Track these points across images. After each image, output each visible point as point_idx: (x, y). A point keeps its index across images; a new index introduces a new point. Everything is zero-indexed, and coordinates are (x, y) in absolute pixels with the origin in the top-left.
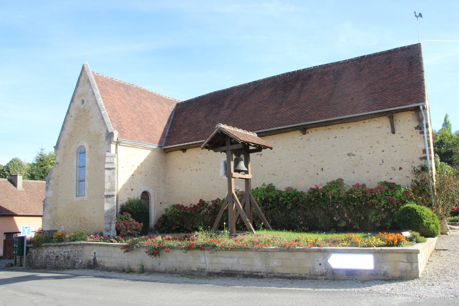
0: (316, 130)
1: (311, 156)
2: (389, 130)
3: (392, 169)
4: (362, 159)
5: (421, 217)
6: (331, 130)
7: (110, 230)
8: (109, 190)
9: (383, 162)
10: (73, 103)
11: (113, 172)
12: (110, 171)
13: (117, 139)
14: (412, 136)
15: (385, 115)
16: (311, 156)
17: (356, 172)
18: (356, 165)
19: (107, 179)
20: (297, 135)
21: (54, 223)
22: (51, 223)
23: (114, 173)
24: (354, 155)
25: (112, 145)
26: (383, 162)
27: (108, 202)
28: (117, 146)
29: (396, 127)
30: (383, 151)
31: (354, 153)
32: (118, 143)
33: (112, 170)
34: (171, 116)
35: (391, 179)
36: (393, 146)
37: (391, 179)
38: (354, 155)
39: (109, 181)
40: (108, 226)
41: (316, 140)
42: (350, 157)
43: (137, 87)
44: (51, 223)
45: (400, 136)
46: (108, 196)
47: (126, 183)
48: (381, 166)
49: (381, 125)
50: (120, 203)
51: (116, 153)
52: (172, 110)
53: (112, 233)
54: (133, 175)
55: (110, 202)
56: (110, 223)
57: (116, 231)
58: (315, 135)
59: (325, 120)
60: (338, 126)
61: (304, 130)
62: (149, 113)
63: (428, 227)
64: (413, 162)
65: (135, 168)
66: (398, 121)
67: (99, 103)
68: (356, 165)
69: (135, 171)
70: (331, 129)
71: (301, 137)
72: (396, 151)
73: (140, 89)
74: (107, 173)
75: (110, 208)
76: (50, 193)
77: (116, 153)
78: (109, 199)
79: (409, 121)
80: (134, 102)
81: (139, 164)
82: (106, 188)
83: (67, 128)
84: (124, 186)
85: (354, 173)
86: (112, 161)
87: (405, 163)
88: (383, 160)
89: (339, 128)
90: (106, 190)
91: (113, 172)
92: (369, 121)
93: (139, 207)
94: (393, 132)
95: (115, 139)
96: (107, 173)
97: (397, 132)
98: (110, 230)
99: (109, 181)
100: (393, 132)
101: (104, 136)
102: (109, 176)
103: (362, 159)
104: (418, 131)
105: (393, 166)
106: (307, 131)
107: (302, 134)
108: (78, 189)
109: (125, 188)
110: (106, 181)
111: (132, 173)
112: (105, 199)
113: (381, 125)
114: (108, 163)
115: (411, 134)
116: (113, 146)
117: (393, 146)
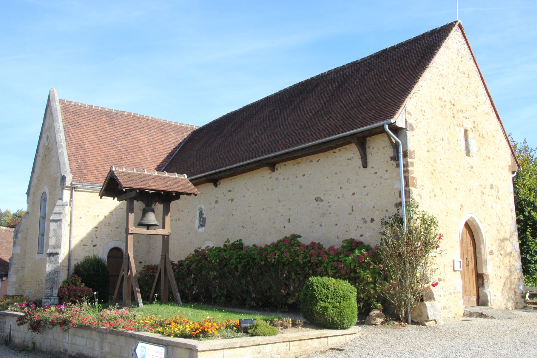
0: (285, 165)
1: (279, 201)
2: (360, 162)
3: (362, 222)
4: (330, 206)
5: (316, 298)
6: (300, 164)
7: (51, 296)
8: (54, 247)
9: (353, 211)
10: (42, 140)
11: (60, 224)
12: (56, 224)
13: (71, 184)
14: (387, 171)
15: (349, 143)
16: (279, 201)
17: (323, 224)
18: (324, 215)
19: (51, 233)
20: (264, 174)
21: (20, 286)
22: (16, 286)
23: (60, 226)
24: (322, 200)
25: (64, 191)
26: (353, 211)
27: (50, 262)
28: (72, 191)
29: (370, 158)
30: (353, 194)
31: (322, 197)
32: (73, 188)
33: (59, 223)
34: (176, 148)
35: (362, 236)
36: (365, 187)
37: (362, 236)
38: (322, 200)
39: (54, 236)
40: (49, 291)
41: (284, 179)
42: (317, 203)
43: (129, 114)
44: (16, 286)
45: (373, 171)
46: (51, 254)
47: (86, 238)
48: (351, 216)
49: (352, 155)
50: (74, 263)
51: (71, 201)
52: (181, 141)
53: (52, 300)
54: (96, 227)
55: (53, 261)
56: (52, 288)
57: (57, 298)
58: (287, 172)
59: (284, 151)
60: (307, 159)
61: (272, 164)
62: (139, 147)
63: (324, 313)
64: (387, 211)
65: (101, 218)
66: (371, 147)
67: (57, 139)
68: (324, 215)
69: (101, 223)
70: (300, 163)
71: (269, 176)
72: (367, 194)
73: (135, 116)
74: (53, 225)
75: (53, 269)
76: (18, 250)
77: (71, 201)
78: (53, 258)
79: (384, 148)
80: (118, 134)
81: (107, 213)
82: (50, 244)
83: (36, 170)
84: (82, 241)
85: (321, 225)
86: (61, 212)
87: (377, 213)
88: (353, 207)
89: (308, 162)
90: (50, 247)
91: (60, 224)
92: (340, 150)
93: (93, 268)
94: (365, 166)
95: (68, 184)
96: (53, 225)
97: (370, 165)
98: (51, 296)
99: (54, 236)
100: (365, 166)
101: (59, 180)
102: (54, 230)
103: (330, 206)
104: (394, 163)
105: (364, 217)
106: (276, 167)
107: (270, 171)
108: (40, 245)
109: (83, 243)
110: (51, 235)
111: (95, 224)
112: (48, 258)
113: (352, 155)
114: (55, 213)
115: (386, 168)
116: (66, 194)
117: (365, 187)
